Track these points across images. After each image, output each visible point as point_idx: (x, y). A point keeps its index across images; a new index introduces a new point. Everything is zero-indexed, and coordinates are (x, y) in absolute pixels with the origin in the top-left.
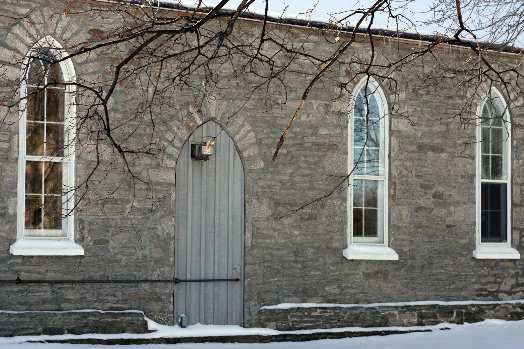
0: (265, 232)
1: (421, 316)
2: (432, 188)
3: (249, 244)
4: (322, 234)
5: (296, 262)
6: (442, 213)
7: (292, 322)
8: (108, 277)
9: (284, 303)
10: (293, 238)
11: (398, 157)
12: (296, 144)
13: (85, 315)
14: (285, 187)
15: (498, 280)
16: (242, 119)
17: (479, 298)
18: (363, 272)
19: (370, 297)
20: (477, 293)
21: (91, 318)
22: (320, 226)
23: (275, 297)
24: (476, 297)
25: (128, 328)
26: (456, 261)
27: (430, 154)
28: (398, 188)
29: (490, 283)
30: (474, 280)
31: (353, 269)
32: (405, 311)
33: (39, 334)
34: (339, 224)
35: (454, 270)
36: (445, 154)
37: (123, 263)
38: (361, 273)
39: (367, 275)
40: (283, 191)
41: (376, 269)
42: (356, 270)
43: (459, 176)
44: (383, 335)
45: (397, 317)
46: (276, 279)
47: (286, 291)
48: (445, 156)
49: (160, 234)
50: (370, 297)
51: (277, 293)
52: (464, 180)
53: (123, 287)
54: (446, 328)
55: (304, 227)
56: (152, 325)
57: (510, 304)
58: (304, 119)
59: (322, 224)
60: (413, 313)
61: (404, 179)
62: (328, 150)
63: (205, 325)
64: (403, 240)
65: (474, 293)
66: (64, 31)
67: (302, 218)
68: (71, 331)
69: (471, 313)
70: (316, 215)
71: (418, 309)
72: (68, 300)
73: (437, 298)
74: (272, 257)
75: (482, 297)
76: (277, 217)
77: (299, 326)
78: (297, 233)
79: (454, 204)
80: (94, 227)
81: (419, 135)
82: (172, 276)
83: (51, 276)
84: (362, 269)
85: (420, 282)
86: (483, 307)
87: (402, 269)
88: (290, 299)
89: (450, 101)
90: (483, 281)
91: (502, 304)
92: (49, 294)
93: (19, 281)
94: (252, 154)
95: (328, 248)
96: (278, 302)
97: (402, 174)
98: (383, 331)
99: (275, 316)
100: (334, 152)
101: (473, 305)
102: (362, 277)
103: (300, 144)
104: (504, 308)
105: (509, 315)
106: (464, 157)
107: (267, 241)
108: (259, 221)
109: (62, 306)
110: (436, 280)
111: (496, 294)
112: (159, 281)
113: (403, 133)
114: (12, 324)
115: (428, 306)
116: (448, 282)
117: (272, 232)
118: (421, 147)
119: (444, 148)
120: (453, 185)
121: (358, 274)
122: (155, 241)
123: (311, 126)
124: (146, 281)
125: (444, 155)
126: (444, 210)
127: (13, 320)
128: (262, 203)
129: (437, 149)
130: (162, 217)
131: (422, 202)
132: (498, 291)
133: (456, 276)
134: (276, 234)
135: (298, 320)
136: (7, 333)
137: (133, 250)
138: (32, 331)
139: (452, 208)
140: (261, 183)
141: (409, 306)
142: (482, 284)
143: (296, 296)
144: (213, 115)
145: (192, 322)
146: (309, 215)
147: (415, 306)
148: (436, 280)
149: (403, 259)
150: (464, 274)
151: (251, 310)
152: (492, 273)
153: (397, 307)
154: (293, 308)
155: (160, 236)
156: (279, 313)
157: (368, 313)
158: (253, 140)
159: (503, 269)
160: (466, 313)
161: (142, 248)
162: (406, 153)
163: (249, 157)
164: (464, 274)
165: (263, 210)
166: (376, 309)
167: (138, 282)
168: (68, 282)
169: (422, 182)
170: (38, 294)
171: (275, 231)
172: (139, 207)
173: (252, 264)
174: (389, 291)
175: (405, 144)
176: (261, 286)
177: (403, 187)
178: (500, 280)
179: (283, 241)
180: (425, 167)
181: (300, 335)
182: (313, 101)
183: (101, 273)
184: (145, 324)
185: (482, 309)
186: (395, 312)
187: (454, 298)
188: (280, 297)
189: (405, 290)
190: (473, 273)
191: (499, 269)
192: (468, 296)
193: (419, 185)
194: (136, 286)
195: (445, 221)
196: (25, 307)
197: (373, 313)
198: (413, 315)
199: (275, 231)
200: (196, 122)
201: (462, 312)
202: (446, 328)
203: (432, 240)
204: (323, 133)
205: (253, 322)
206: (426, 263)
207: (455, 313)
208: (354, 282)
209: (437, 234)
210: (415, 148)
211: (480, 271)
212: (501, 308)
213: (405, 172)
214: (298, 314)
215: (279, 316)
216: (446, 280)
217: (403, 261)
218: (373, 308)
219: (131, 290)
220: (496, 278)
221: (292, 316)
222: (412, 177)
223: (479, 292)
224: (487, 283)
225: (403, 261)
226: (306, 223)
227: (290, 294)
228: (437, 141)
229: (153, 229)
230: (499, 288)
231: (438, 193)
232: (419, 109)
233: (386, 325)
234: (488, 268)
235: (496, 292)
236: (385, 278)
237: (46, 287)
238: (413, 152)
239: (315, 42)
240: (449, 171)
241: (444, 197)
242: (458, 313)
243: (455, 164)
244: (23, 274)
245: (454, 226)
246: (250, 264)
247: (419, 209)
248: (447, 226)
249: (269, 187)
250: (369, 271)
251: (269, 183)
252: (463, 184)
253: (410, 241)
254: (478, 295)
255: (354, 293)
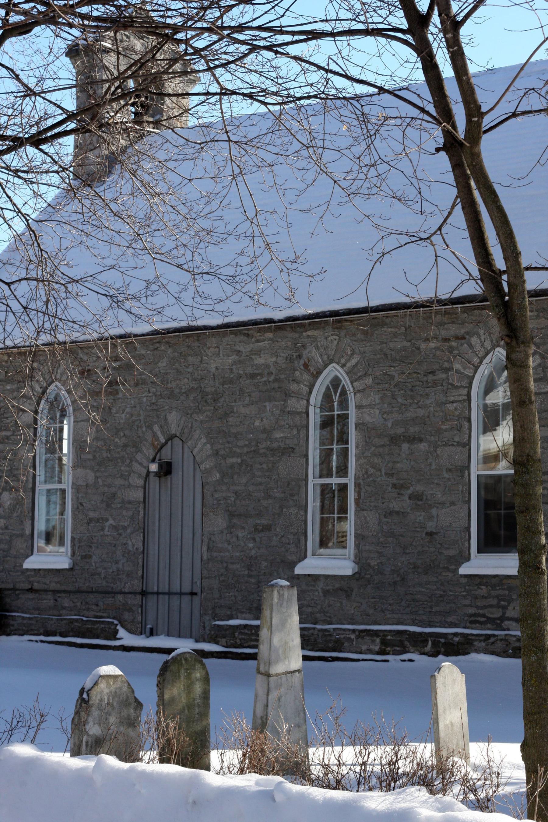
0: (220, 545)
1: (384, 642)
2: (408, 488)
3: (205, 558)
4: (276, 546)
5: (250, 576)
6: (421, 518)
7: (240, 639)
8: (92, 588)
9: (238, 618)
10: (248, 551)
11: (363, 454)
12: (251, 452)
13: (72, 621)
14: (240, 498)
15: (502, 603)
16: (198, 432)
17: (474, 626)
18: (322, 588)
19: (330, 617)
20: (471, 619)
21: (76, 624)
22: (274, 538)
23: (229, 613)
24: (468, 625)
25: (102, 635)
26: (440, 577)
27: (405, 446)
28: (364, 490)
29: (491, 606)
30: (467, 602)
31: (311, 585)
32: (364, 636)
33: (40, 635)
34: (294, 535)
35: (438, 589)
36: (425, 444)
37: (103, 576)
38: (320, 590)
39: (326, 593)
40: (238, 502)
41: (337, 586)
42: (314, 586)
43: (444, 471)
44: (330, 661)
45: (354, 643)
46: (231, 594)
47: (240, 607)
48: (424, 446)
49: (130, 548)
50: (330, 617)
51: (230, 608)
52: (450, 474)
53: (104, 597)
54: (410, 660)
55: (258, 540)
56: (122, 633)
57: (511, 635)
58: (258, 424)
59: (276, 535)
60: (375, 638)
61: (371, 479)
62: (283, 454)
63: (167, 637)
64: (369, 551)
65: (466, 618)
66: (62, 375)
67: (256, 530)
68: (62, 635)
69: (453, 644)
70: (271, 526)
71: (381, 634)
72: (64, 608)
73: (414, 624)
74: (226, 570)
75: (477, 625)
76: (231, 528)
77: (246, 645)
78: (251, 545)
79: (437, 505)
80: (82, 544)
81: (390, 425)
82: (140, 589)
83: (53, 586)
84: (321, 585)
85: (391, 602)
86: (473, 638)
87: (369, 586)
88: (244, 615)
89: (431, 377)
90: (479, 604)
91: (501, 635)
92: (52, 601)
93: (31, 590)
94: (208, 466)
95: (282, 561)
96: (231, 617)
97: (369, 473)
98: (331, 657)
99: (223, 632)
100: (289, 456)
101: (456, 634)
102: (321, 594)
103: (254, 451)
104: (501, 640)
105: (510, 651)
106: (452, 445)
107: (222, 554)
108: (214, 534)
109: (61, 612)
110: (413, 600)
111: (498, 622)
112: (130, 593)
113: (369, 425)
114: (24, 625)
115: (394, 631)
116: (429, 604)
117: (226, 545)
118: (395, 440)
119: (423, 436)
120: (436, 481)
121: (317, 590)
122: (126, 555)
123: (264, 431)
124: (121, 593)
125: (423, 446)
126: (423, 514)
127: (25, 622)
128: (217, 515)
129: (413, 440)
130: (132, 533)
131: (395, 505)
132: (503, 618)
133: (441, 596)
134: (230, 548)
135: (246, 637)
136: (21, 632)
137: (110, 564)
138: (36, 632)
139: (434, 511)
140: (217, 495)
141: (369, 630)
142: (477, 607)
143: (250, 613)
144: (173, 432)
145: (159, 633)
146: (263, 526)
147: (377, 630)
148: (413, 600)
149: (369, 574)
150: (451, 593)
151: (206, 625)
152: (493, 593)
153: (354, 631)
154: (240, 625)
155: (130, 551)
156: (226, 630)
157: (320, 634)
158: (210, 452)
159: (510, 589)
160: (445, 644)
161: (117, 562)
162: (373, 448)
163: (206, 469)
164: (451, 593)
165: (219, 522)
166: (329, 631)
167: (115, 593)
168: (65, 592)
169: (395, 481)
170: (45, 601)
171: (229, 544)
172: (114, 524)
173: (208, 578)
174: (352, 612)
175: (372, 438)
176: (216, 601)
177: (369, 489)
178: (506, 603)
179: (238, 554)
180: (398, 462)
181: (241, 653)
182: (267, 404)
183: (87, 585)
184: (117, 632)
185: (470, 639)
186: (353, 636)
187: (438, 625)
188: (234, 613)
189: (371, 611)
190: (464, 593)
191: (504, 589)
192: (457, 622)
193: (391, 485)
194: (113, 597)
195: (425, 528)
196: (37, 612)
197: (326, 635)
198: (373, 641)
199: (229, 544)
200: (159, 441)
201: (439, 642)
202: (410, 660)
203: (408, 551)
204: (278, 436)
205: (206, 637)
206: (398, 579)
207: (430, 643)
208: (313, 599)
209: (414, 543)
210: (386, 440)
211: (476, 590)
212: (497, 640)
213: (371, 471)
214: (246, 631)
215: (228, 632)
216: (426, 601)
217: (369, 576)
218: (326, 630)
219: (110, 601)
220: (500, 600)
221: (241, 633)
222: (381, 476)
223: (474, 619)
224: (485, 607)
225: (369, 576)
226: (260, 535)
227: (245, 610)
228: (413, 430)
229: (125, 544)
230: (504, 614)
231: (415, 494)
232: (389, 393)
233: (341, 651)
234: (487, 586)
235: (499, 619)
236: (348, 596)
237: (50, 596)
238: (383, 446)
239: (271, 340)
240: (430, 465)
241: (425, 498)
242: (433, 643)
243: (438, 455)
244: (35, 584)
245: (436, 534)
246: (206, 578)
247: (390, 513)
248: (427, 534)
249: (225, 499)
250: (328, 588)
251: (224, 495)
252: (449, 479)
253: (378, 552)
254: (471, 622)
255: (311, 612)
